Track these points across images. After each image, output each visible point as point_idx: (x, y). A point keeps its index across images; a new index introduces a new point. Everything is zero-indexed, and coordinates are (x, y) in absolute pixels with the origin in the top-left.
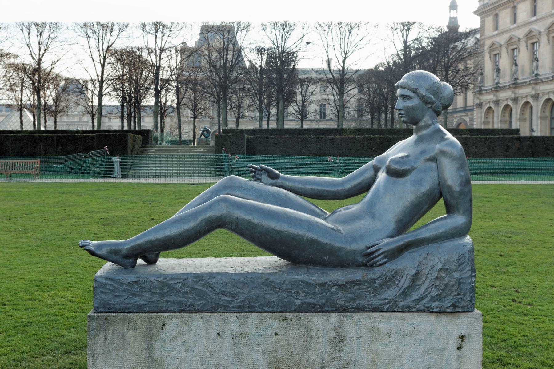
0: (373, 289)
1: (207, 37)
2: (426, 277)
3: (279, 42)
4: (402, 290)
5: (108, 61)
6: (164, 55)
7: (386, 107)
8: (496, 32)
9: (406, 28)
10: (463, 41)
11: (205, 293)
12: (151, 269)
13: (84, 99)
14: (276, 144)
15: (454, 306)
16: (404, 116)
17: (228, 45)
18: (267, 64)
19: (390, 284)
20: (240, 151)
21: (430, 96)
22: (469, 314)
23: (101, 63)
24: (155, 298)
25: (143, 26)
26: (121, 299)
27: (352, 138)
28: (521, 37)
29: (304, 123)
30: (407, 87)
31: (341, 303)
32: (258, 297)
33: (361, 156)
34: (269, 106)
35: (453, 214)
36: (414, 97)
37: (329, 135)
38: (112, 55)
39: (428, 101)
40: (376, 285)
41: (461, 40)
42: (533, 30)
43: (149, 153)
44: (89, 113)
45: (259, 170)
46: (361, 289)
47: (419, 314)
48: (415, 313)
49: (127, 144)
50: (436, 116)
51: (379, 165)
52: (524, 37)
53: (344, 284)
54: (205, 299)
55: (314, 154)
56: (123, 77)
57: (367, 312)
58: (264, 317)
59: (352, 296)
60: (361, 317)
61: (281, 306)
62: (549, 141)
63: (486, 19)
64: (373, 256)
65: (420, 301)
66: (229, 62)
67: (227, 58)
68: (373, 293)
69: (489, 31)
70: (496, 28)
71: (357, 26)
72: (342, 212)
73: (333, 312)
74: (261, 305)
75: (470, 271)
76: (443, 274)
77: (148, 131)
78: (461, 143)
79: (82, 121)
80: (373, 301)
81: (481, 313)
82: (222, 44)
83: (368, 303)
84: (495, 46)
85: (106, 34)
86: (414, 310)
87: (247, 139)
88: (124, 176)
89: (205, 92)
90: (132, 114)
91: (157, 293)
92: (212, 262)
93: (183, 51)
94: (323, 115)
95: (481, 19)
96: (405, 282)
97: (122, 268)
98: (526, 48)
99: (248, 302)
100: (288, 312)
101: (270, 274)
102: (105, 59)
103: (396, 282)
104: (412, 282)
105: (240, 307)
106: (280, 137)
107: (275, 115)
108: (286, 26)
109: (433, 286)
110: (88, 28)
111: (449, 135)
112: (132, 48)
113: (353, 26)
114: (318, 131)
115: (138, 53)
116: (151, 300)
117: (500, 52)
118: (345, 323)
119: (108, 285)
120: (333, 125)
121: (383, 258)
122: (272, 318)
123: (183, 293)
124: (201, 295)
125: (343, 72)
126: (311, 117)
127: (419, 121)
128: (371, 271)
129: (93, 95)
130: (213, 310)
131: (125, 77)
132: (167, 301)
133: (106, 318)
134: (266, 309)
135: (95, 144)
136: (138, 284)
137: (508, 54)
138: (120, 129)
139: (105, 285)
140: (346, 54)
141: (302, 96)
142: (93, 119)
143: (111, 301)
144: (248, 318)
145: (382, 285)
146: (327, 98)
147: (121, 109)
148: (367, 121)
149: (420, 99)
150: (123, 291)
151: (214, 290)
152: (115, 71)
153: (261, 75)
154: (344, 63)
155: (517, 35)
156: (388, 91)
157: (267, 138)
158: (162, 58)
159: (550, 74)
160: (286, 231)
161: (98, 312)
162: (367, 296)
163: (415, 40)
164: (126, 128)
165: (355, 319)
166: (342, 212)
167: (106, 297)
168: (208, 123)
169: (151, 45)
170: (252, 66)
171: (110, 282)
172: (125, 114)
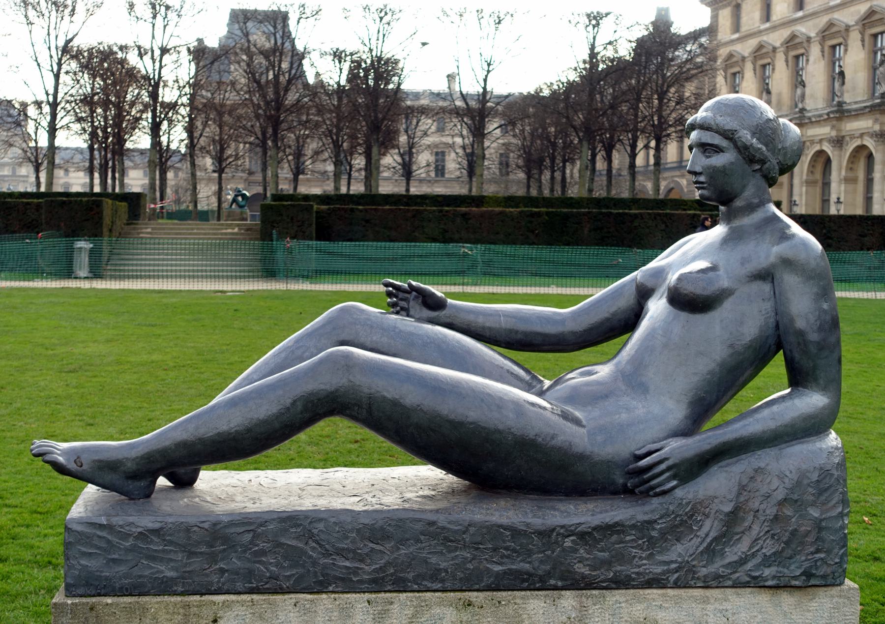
0: (648, 541)
1: (246, 28)
2: (754, 516)
3: (374, 42)
4: (705, 545)
5: (65, 68)
6: (166, 58)
7: (553, 160)
8: (736, 36)
9: (594, 22)
10: (688, 48)
11: (303, 552)
12: (183, 499)
13: (21, 136)
14: (367, 221)
15: (808, 574)
16: (705, 185)
17: (283, 44)
18: (349, 80)
19: (682, 532)
20: (304, 232)
21: (760, 146)
22: (835, 591)
23: (52, 71)
24: (196, 564)
25: (130, 6)
26: (122, 569)
27: (501, 213)
28: (778, 44)
29: (411, 185)
30: (714, 128)
31: (583, 570)
32: (414, 559)
33: (515, 244)
34: (351, 154)
35: (805, 387)
36: (728, 149)
37: (459, 206)
38: (72, 57)
39: (755, 156)
40: (654, 534)
41: (686, 45)
42: (798, 34)
43: (141, 235)
44: (32, 162)
45: (404, 291)
46: (623, 542)
47: (738, 590)
48: (730, 590)
49: (101, 218)
50: (767, 186)
51: (649, 284)
52: (782, 45)
53: (589, 533)
54: (303, 566)
55: (434, 240)
56: (92, 98)
57: (634, 587)
58: (425, 601)
59: (606, 555)
60: (622, 599)
61: (461, 579)
62: (832, 224)
63: (720, 12)
64: (650, 474)
65: (742, 565)
66: (283, 74)
67: (280, 67)
68: (648, 549)
69: (725, 33)
70: (736, 28)
71: (509, 16)
72: (575, 379)
73: (566, 589)
74: (418, 576)
75: (841, 505)
76: (788, 511)
77: (138, 196)
78: (822, 244)
79: (18, 174)
80: (647, 567)
81: (856, 586)
82: (273, 42)
83: (636, 570)
84: (735, 59)
85: (62, 19)
86: (730, 583)
87: (317, 212)
88: (96, 273)
89: (240, 127)
90: (108, 164)
91: (201, 553)
92: (310, 481)
93: (199, 53)
94: (440, 170)
95: (712, 11)
96: (710, 528)
97: (123, 497)
98: (784, 64)
99: (392, 571)
100: (474, 590)
101: (437, 511)
102: (60, 65)
103: (694, 528)
104: (725, 528)
105: (374, 581)
106: (375, 209)
107: (361, 169)
108: (386, 14)
109: (768, 535)
110: (30, 7)
111: (796, 228)
112: (109, 47)
113: (502, 17)
114: (439, 199)
115: (120, 55)
116: (188, 569)
117: (743, 70)
118: (590, 612)
119: (95, 538)
120: (459, 190)
121: (668, 480)
122: (440, 604)
123: (257, 554)
124: (294, 556)
125: (484, 95)
126: (420, 172)
127: (735, 197)
128: (644, 504)
129: (37, 129)
130: (320, 586)
131: (96, 98)
132: (222, 571)
133: (92, 609)
134: (429, 585)
135: (43, 217)
136: (159, 536)
137: (755, 74)
138: (88, 190)
139: (88, 538)
140: (489, 65)
141: (409, 137)
142: (37, 171)
143: (102, 572)
144: (392, 603)
145: (665, 534)
146: (451, 142)
147: (88, 154)
148: (519, 182)
149: (739, 151)
150: (128, 550)
151: (321, 546)
152: (78, 85)
153: (340, 99)
154: (485, 80)
155: (770, 42)
156: (555, 132)
157: (352, 210)
158: (163, 64)
159: (823, 109)
160: (471, 423)
161: (74, 596)
162: (635, 557)
163: (607, 44)
164: (97, 189)
165: (611, 603)
166: (575, 379)
167: (93, 564)
168: (242, 181)
169: (146, 44)
170: (321, 84)
171: (99, 533)
172: (96, 163)
